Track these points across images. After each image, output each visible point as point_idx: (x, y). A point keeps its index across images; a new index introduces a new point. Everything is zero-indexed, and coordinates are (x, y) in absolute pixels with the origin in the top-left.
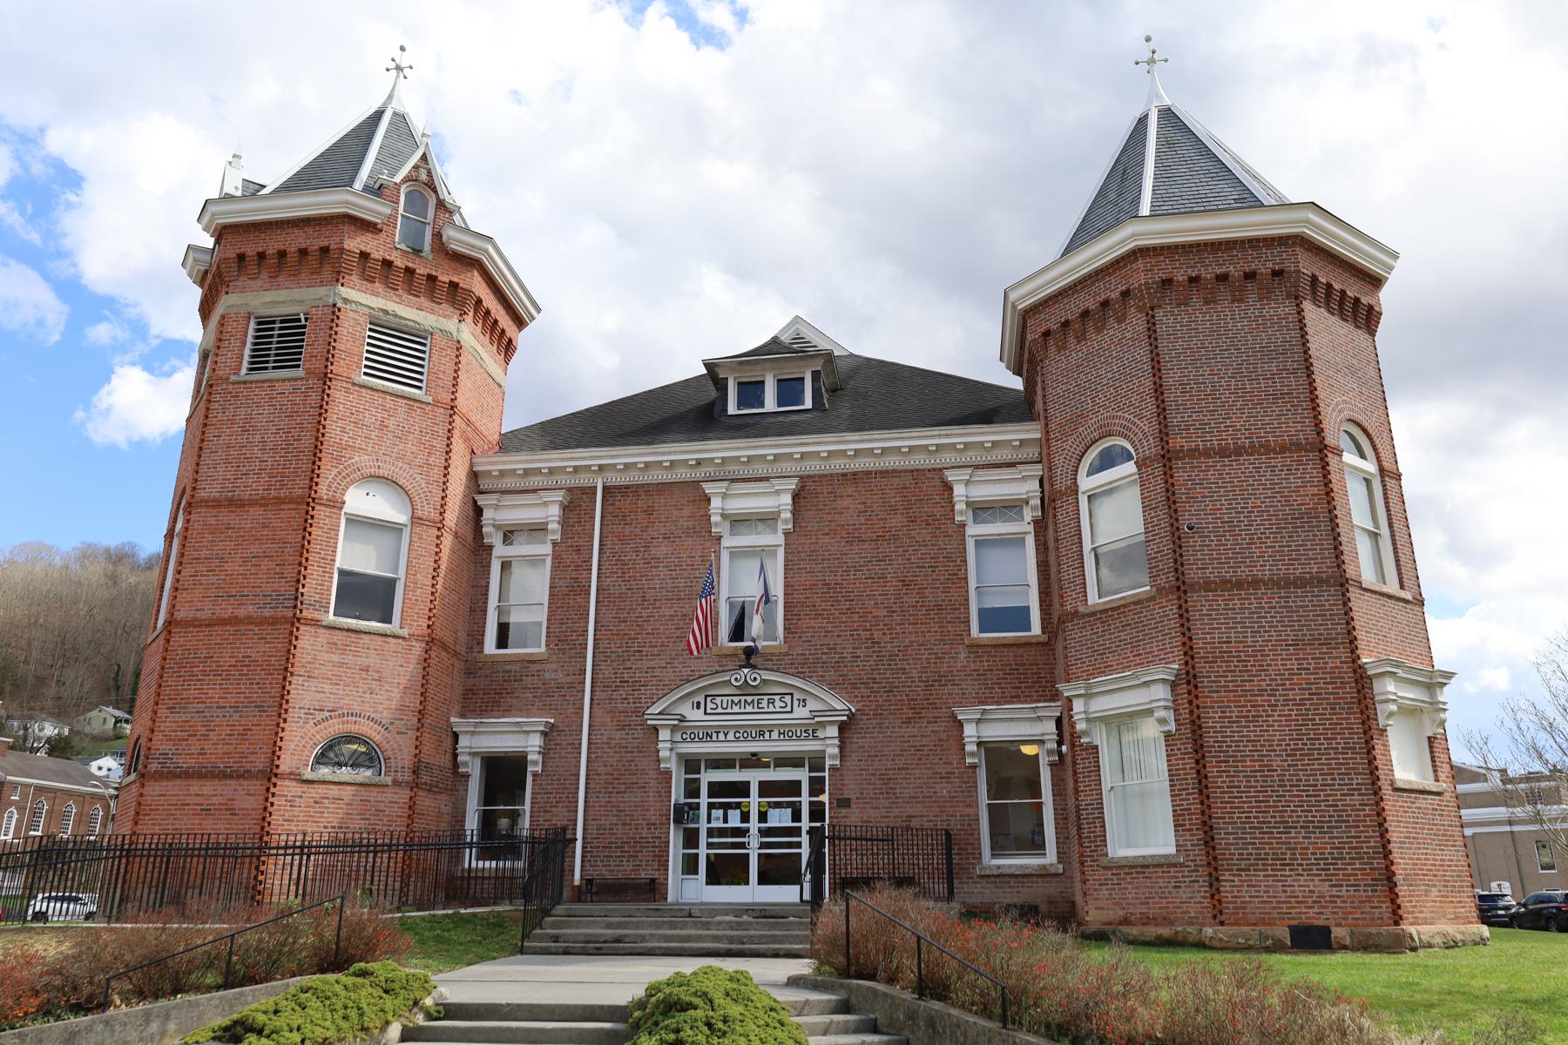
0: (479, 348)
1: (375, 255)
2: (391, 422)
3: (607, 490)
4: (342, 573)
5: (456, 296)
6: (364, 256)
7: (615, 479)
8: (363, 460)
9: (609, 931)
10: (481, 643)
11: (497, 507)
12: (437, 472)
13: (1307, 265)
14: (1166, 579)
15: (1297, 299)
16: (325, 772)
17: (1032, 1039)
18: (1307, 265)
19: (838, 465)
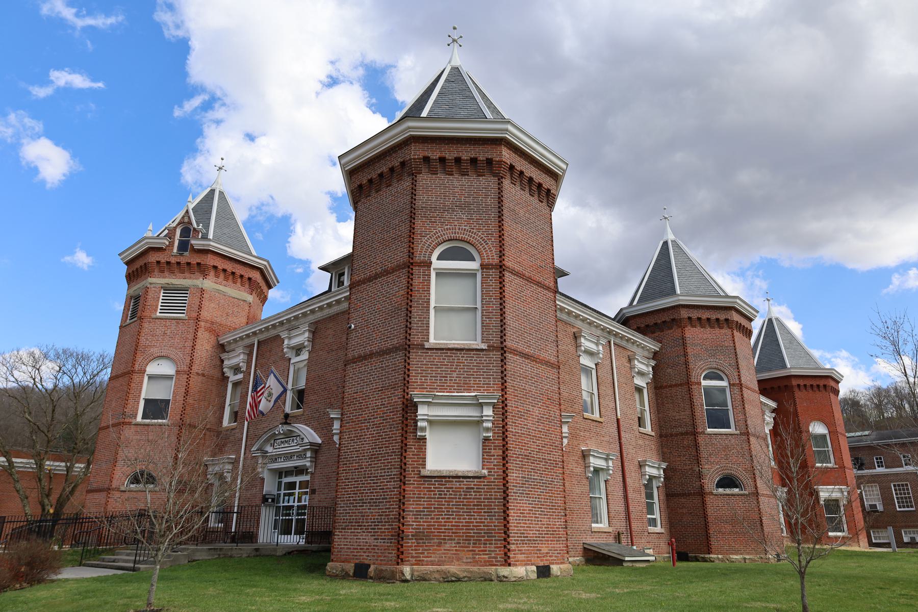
0: (221, 288)
1: (163, 261)
2: (168, 332)
3: (259, 342)
4: (147, 401)
5: (202, 269)
6: (158, 262)
7: (262, 337)
8: (155, 351)
9: (475, 569)
10: (221, 423)
11: (229, 359)
12: (188, 350)
13: (507, 155)
14: (495, 341)
15: (501, 179)
16: (721, 490)
17: (439, 610)
18: (507, 155)
19: (327, 312)
